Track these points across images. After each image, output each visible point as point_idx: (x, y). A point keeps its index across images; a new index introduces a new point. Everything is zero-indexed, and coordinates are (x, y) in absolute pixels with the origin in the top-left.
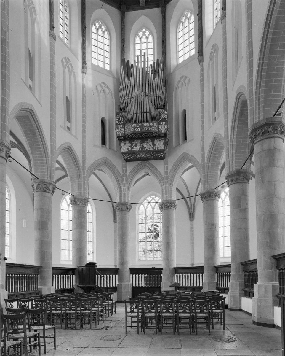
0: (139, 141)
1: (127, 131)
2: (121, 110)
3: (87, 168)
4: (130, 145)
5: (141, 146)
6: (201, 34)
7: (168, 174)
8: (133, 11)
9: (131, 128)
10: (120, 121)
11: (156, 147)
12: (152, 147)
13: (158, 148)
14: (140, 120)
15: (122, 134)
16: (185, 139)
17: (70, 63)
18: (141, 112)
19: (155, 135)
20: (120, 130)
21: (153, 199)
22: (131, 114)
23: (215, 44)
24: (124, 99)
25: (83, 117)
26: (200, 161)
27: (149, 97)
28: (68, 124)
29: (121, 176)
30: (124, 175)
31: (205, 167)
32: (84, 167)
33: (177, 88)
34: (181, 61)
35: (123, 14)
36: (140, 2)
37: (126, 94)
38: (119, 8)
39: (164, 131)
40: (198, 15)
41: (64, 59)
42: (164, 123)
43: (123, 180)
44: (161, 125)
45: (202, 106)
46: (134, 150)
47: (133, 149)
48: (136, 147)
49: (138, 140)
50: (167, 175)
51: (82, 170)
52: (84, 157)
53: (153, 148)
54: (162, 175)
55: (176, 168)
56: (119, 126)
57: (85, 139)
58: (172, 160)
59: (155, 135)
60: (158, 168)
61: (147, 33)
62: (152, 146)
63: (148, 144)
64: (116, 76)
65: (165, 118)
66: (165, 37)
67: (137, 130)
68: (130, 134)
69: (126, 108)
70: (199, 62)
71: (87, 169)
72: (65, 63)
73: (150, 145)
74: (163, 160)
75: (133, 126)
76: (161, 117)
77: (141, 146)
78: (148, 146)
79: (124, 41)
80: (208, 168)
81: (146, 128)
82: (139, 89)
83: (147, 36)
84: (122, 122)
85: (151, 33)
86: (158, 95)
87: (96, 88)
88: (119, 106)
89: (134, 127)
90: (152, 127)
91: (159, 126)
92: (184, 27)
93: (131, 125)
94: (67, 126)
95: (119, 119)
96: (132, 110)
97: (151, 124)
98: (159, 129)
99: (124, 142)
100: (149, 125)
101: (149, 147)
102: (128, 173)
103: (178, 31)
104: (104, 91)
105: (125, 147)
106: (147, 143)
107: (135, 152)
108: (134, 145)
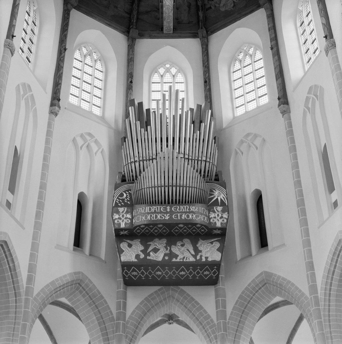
0: (164, 241)
1: (138, 219)
2: (123, 180)
3: (35, 293)
4: (142, 248)
5: (168, 252)
6: (280, 73)
7: (228, 318)
8: (151, 38)
9: (148, 213)
10: (123, 200)
11: (201, 256)
12: (192, 255)
13: (206, 258)
14: (172, 200)
15: (126, 224)
16: (263, 243)
17: (31, 93)
18: (171, 184)
19: (200, 230)
20: (121, 216)
21: (168, 70)
22: (150, 186)
23: (315, 85)
24: (132, 160)
25: (41, 188)
26: (305, 289)
28: (9, 196)
29: (113, 317)
30: (122, 315)
31: (322, 303)
32: (29, 291)
33: (237, 153)
34: (240, 112)
35: (132, 41)
36: (164, 27)
37: (138, 153)
38: (127, 32)
39: (221, 223)
40: (272, 49)
41: (21, 86)
42: (220, 208)
43: (118, 326)
44: (214, 212)
45: (298, 183)
46: (152, 258)
47: (148, 258)
48: (156, 253)
49: (160, 239)
50: (226, 319)
51: (23, 297)
52: (32, 269)
53: (195, 256)
54: (212, 321)
55: (244, 307)
56: (121, 210)
57: (40, 230)
58: (233, 289)
59: (200, 230)
60: (202, 303)
61: (174, 71)
62: (193, 253)
63: (183, 248)
64: (113, 125)
65: (221, 199)
66: (209, 76)
67: (160, 217)
68: (146, 225)
70: (282, 113)
71: (34, 295)
72: (22, 93)
73: (188, 250)
74: (213, 286)
75: (153, 210)
76: (212, 196)
77: (168, 252)
78: (184, 253)
79: (133, 76)
80: (329, 306)
81: (181, 216)
82: (165, 146)
84: (128, 201)
85: (181, 70)
86: (205, 158)
88: (119, 173)
89: (155, 211)
90: (197, 214)
91: (209, 213)
92: (242, 66)
93: (147, 208)
94: (7, 200)
95: (122, 195)
96: (151, 180)
97: (193, 208)
98: (210, 219)
99: (128, 241)
100: (189, 209)
101: (187, 254)
102: (129, 313)
103: (232, 71)
105: (131, 253)
106: (183, 245)
107: (154, 264)
108: (150, 249)
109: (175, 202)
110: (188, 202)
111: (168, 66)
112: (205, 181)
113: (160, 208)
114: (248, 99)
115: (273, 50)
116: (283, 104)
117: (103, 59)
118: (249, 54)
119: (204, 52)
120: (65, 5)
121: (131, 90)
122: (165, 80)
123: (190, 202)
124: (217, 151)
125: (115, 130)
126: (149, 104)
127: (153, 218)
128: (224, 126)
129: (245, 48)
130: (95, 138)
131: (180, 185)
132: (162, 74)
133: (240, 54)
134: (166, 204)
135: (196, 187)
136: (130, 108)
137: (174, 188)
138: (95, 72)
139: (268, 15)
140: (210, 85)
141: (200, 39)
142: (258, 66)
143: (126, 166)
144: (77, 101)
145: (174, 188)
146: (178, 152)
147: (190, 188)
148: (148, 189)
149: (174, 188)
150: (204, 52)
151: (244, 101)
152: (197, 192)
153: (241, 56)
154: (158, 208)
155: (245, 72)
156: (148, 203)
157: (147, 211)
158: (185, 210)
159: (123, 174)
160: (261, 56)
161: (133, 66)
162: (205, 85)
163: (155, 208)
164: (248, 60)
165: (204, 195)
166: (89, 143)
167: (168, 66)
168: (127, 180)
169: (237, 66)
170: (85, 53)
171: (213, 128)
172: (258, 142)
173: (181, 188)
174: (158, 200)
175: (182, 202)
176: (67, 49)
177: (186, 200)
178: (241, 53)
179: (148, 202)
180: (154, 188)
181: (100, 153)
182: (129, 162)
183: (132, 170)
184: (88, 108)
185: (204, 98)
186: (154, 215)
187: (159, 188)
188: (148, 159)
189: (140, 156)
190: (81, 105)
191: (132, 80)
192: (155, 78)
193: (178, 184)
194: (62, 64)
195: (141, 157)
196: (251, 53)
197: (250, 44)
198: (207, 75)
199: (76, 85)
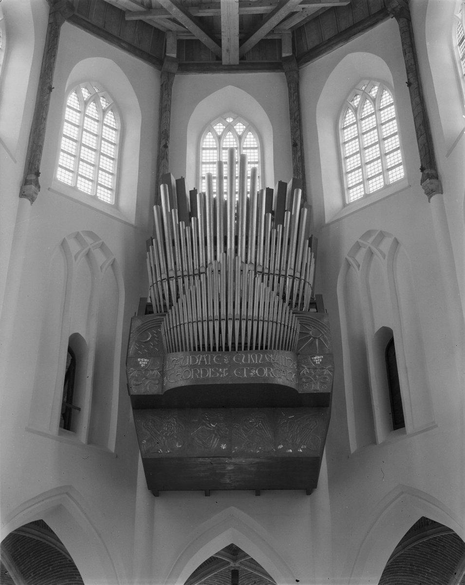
16: (397, 421)
21: (229, 128)
27: (266, 277)
33: (349, 265)
34: (355, 195)
40: (409, 84)
69: (171, 305)
83: (240, 134)
85: (252, 126)
87: (62, 244)
92: (359, 118)
96: (192, 314)
103: (340, 126)
104: (88, 255)
109: (238, 347)
110: (262, 348)
111: (230, 120)
112: (291, 312)
113: (212, 358)
114: (369, 173)
115: (412, 86)
116: (430, 178)
117: (117, 108)
118: (370, 97)
119: (292, 96)
120: (51, 15)
121: (165, 160)
122: (224, 143)
123: (264, 347)
124: (313, 260)
125: (136, 227)
126: (197, 183)
127: (199, 375)
128: (327, 221)
129: (364, 88)
130: (102, 241)
131: (241, 317)
132: (219, 134)
133: (356, 97)
134: (222, 350)
135: (275, 320)
136: (162, 187)
137: (237, 324)
138: (104, 131)
139: (402, 28)
140: (302, 150)
141: (286, 73)
142: (386, 117)
143: (153, 286)
144: (70, 178)
145: (236, 322)
146: (244, 260)
147: (266, 324)
148: (190, 325)
149: (237, 324)
150: (292, 96)
151: (361, 177)
152: (278, 330)
153: (356, 102)
154: (207, 358)
155: (364, 128)
156: (190, 350)
157: (189, 362)
158: (255, 361)
159: (149, 301)
160: (391, 99)
161: (168, 119)
162: (293, 151)
163: (203, 358)
164: (368, 108)
165: (290, 337)
166: (89, 250)
167: (230, 120)
168: (155, 311)
169: (350, 117)
170: (86, 97)
171: (307, 216)
172: (386, 245)
173: (250, 323)
174: (209, 345)
175: (251, 348)
176: (54, 88)
177: (257, 344)
178: (356, 95)
179: (186, 347)
180: (201, 323)
181: (110, 267)
182: (159, 279)
183: (164, 295)
184: (90, 191)
185: (292, 172)
186: (200, 371)
187: (211, 324)
188: (191, 273)
189: (178, 269)
190: (78, 186)
191: (167, 142)
192: (208, 140)
193: (230, 316)
194: (44, 114)
195: (179, 270)
196: (374, 95)
197: (372, 80)
198: (298, 133)
199: (69, 152)
